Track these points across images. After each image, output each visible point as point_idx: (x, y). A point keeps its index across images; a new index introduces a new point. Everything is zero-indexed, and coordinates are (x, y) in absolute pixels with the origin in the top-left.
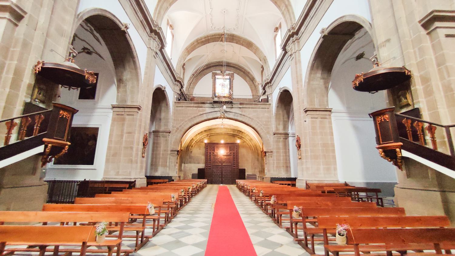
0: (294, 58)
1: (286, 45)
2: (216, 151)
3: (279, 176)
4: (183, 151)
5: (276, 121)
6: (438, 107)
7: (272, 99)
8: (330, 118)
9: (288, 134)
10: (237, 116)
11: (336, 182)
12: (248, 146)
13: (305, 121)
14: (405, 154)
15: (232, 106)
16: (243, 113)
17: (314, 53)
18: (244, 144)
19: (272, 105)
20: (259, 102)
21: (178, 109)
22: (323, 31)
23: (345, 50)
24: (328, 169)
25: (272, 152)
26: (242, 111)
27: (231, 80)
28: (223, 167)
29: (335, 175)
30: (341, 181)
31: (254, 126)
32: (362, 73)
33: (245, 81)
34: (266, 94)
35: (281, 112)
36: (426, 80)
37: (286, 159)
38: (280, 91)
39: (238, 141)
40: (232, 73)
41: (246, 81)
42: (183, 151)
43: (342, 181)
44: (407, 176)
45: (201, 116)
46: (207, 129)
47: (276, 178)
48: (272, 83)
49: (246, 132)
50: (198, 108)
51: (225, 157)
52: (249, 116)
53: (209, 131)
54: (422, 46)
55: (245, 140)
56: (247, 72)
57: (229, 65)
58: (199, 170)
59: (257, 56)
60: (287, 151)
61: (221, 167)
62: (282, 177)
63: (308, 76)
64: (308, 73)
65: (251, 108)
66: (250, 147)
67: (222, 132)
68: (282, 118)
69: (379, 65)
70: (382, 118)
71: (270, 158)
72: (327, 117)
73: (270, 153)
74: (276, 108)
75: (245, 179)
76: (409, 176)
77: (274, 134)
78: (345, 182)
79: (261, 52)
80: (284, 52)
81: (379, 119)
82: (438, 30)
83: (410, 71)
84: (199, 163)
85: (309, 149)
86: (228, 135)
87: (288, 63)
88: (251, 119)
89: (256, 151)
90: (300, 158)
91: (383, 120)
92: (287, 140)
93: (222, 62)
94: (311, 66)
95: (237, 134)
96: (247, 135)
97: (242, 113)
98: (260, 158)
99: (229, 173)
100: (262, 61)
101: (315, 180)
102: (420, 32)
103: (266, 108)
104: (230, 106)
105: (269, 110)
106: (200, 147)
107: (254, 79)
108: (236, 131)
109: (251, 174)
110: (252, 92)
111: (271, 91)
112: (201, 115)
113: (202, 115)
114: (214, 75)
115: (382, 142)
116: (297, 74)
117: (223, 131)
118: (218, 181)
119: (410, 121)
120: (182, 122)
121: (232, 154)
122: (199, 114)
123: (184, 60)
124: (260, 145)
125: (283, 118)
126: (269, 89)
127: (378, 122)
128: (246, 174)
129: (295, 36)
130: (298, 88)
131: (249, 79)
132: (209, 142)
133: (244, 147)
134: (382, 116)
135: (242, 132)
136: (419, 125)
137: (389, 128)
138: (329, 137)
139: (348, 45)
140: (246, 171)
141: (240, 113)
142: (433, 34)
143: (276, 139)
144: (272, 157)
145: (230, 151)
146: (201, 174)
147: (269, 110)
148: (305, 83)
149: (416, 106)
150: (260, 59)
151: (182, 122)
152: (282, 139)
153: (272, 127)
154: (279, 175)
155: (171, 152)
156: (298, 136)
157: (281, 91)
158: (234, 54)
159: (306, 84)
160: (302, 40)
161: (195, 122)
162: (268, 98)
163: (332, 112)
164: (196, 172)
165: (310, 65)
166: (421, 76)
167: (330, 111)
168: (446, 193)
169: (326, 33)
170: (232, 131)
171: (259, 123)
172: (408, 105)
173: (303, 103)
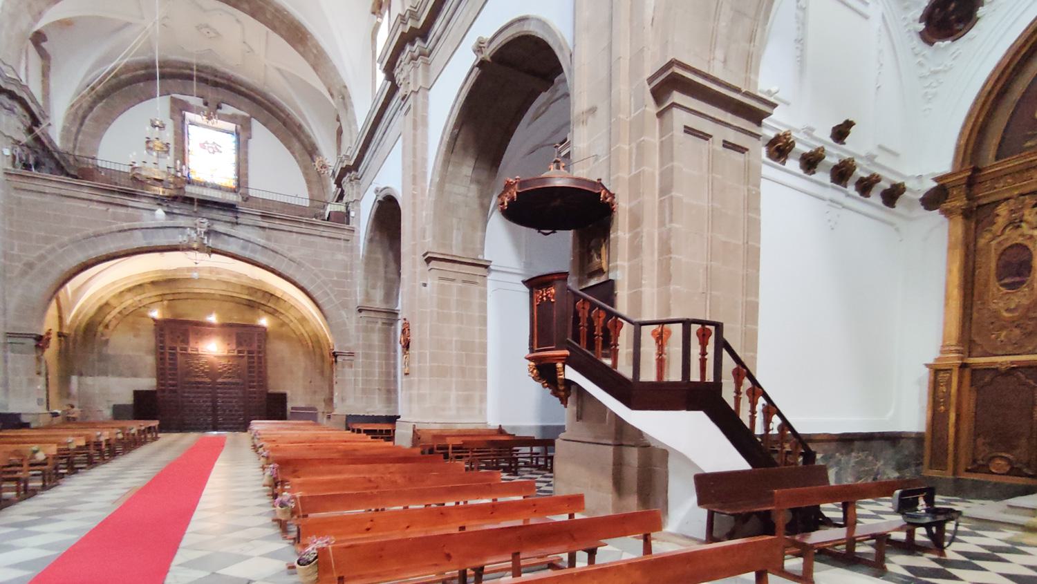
0: (412, 110)
1: (395, 65)
2: (192, 344)
3: (368, 413)
4: (71, 339)
5: (366, 278)
6: (643, 282)
7: (357, 217)
8: (485, 285)
9: (397, 314)
10: (254, 251)
11: (481, 427)
12: (295, 336)
13: (425, 285)
14: (571, 374)
15: (237, 218)
16: (272, 245)
17: (457, 105)
18: (284, 329)
19: (359, 232)
20: (324, 220)
21: (23, 197)
22: (481, 47)
23: (536, 117)
24: (467, 400)
25: (351, 354)
26: (268, 239)
27: (242, 139)
28: (218, 388)
29: (482, 411)
30: (492, 425)
31: (304, 283)
32: (518, 177)
33: (288, 152)
34: (345, 199)
35: (380, 256)
36: (636, 221)
37: (388, 374)
38: (376, 199)
39: (264, 321)
40: (244, 117)
41: (293, 153)
42: (71, 339)
43: (493, 422)
44: (577, 417)
45: (122, 234)
46: (161, 279)
47: (359, 416)
48: (362, 171)
49: (289, 297)
50: (112, 209)
51: (224, 362)
52: (290, 255)
53: (166, 285)
54: (643, 140)
55: (287, 321)
56: (295, 123)
57: (233, 85)
58: (138, 394)
59: (320, 77)
60: (392, 353)
61: (210, 388)
62: (376, 415)
63: (439, 168)
64: (441, 158)
65: (297, 233)
66: (300, 340)
67: (213, 292)
68: (381, 270)
69: (561, 168)
70: (545, 294)
71: (347, 369)
72: (478, 280)
73: (346, 358)
74: (366, 242)
75: (285, 418)
76: (579, 417)
77: (360, 311)
78: (500, 426)
79: (334, 68)
80: (389, 83)
81: (542, 294)
82: (675, 111)
83: (613, 196)
84: (135, 375)
85: (428, 352)
86: (233, 302)
87: (398, 123)
88: (295, 265)
89: (317, 350)
90: (406, 372)
91: (545, 299)
92: (393, 327)
93: (188, 66)
94: (449, 143)
95: (262, 302)
96: (292, 306)
97: (270, 243)
98: (327, 366)
99: (236, 402)
100: (336, 99)
101: (435, 423)
102: (646, 106)
103: (340, 239)
104: (229, 216)
105: (349, 245)
106: (138, 329)
107: (317, 149)
108: (260, 294)
109: (303, 406)
110: (310, 189)
111: (358, 194)
112: (125, 230)
113: (128, 233)
114: (179, 109)
115: (538, 347)
116: (415, 155)
117: (217, 290)
118: (201, 424)
119: (587, 307)
120: (48, 247)
121: (245, 354)
122: (114, 227)
123: (36, 20)
124: (328, 336)
125: (386, 272)
126: (352, 185)
127: (537, 302)
128: (289, 406)
129: (418, 43)
130: (414, 196)
131: (302, 147)
132: (168, 316)
133: (281, 337)
134: (544, 290)
135: (278, 298)
136: (599, 317)
137: (553, 317)
138: (477, 328)
139: (539, 108)
140: (289, 400)
141: (263, 242)
142: (667, 115)
143: (365, 324)
144: (351, 366)
145: (237, 347)
146: (144, 405)
147: (349, 245)
148: (431, 186)
149: (611, 277)
150: (329, 91)
151: (48, 247)
152: (379, 325)
153: (356, 292)
154: (368, 410)
155: (9, 340)
156: (405, 319)
157: (380, 198)
158: (248, 52)
159: (433, 189)
160: (437, 58)
161: (103, 250)
162: (348, 212)
163: (492, 270)
164: (128, 399)
165: (446, 139)
166: (631, 210)
167: (486, 267)
168: (624, 448)
169: (487, 54)
170: (247, 292)
171: (319, 278)
172: (600, 271)
173: (424, 237)
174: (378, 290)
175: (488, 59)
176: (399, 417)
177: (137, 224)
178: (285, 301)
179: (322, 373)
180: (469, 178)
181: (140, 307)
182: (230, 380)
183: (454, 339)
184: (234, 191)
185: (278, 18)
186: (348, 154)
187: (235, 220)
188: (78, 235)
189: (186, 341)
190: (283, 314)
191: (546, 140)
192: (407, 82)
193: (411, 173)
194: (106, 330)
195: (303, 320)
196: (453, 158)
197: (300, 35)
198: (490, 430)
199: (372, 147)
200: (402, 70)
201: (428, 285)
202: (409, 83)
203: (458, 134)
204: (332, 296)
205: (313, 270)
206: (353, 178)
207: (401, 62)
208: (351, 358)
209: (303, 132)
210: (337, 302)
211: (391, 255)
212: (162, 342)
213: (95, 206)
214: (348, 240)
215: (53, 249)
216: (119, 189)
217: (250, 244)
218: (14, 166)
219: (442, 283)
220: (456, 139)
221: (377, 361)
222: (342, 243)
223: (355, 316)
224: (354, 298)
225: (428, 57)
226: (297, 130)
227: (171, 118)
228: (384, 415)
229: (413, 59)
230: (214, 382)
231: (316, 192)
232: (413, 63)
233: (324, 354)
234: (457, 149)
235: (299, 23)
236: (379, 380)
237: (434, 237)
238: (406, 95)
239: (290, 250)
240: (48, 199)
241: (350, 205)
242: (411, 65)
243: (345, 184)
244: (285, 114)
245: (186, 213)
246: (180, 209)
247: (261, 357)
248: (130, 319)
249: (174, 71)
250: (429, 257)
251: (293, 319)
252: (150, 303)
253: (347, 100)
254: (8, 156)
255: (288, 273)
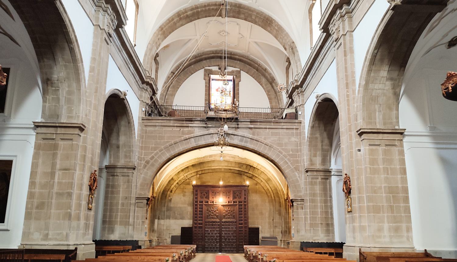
3: (314, 241)
5: (310, 151)
8: (402, 146)
11: (410, 251)
13: (359, 150)
15: (238, 124)
16: (255, 137)
18: (257, 186)
19: (304, 123)
24: (397, 229)
25: (302, 200)
26: (254, 134)
28: (223, 225)
29: (409, 239)
31: (273, 157)
34: (295, 105)
35: (318, 135)
40: (237, 71)
52: (265, 142)
53: (199, 165)
55: (259, 181)
57: (233, 56)
61: (218, 225)
63: (364, 76)
64: (366, 69)
65: (269, 128)
66: (267, 193)
67: (221, 167)
73: (299, 203)
77: (307, 172)
78: (426, 250)
84: (182, 218)
88: (268, 147)
89: (277, 199)
90: (349, 210)
92: (328, 181)
101: (375, 247)
104: (234, 125)
105: (298, 132)
107: (275, 80)
108: (244, 166)
110: (271, 103)
111: (303, 100)
114: (208, 73)
117: (223, 166)
125: (322, 145)
126: (299, 96)
132: (199, 184)
135: (254, 168)
138: (399, 176)
140: (260, 232)
141: (251, 136)
147: (298, 132)
148: (359, 87)
150: (284, 47)
152: (319, 180)
153: (304, 159)
154: (315, 238)
156: (346, 174)
157: (319, 101)
160: (357, 14)
161: (177, 151)
162: (297, 112)
164: (178, 233)
165: (369, 57)
167: (402, 134)
171: (282, 153)
174: (318, 157)
175: (400, 3)
176: (344, 243)
177: (192, 135)
178: (258, 169)
179: (280, 214)
180: (385, 78)
181: (187, 180)
182: (229, 220)
183: (383, 185)
184: (232, 111)
185: (258, 17)
186: (296, 79)
187: (237, 126)
188: (167, 144)
189: (208, 197)
190: (257, 177)
191: (440, 41)
192: (338, 30)
193: (345, 82)
194: (171, 193)
195: (268, 180)
196: (374, 68)
197: (269, 22)
198: (418, 253)
199: (312, 72)
200: (334, 24)
201: (361, 151)
202: (339, 31)
203: (377, 53)
204: (289, 164)
205: (278, 149)
206: (299, 92)
207: (334, 20)
208: (302, 203)
209: (267, 72)
210: (292, 167)
211: (325, 135)
212: (196, 198)
213: (175, 129)
214: (298, 129)
215: (157, 153)
216: (185, 118)
217: (245, 138)
218: (146, 116)
219: (371, 148)
220: (375, 56)
221: (319, 204)
222: (294, 131)
223: (303, 175)
224: (302, 164)
225: (351, 13)
226: (264, 72)
227: (204, 79)
228: (325, 242)
229: (341, 17)
230: (221, 222)
231: (274, 104)
232: (342, 19)
233: (281, 201)
234: (377, 61)
235: (269, 16)
236: (321, 217)
237: (364, 119)
238: (338, 38)
239: (265, 139)
240: (157, 128)
241: (298, 108)
242: (341, 20)
243: (294, 96)
244: (257, 64)
245: (214, 126)
246: (211, 124)
247: (246, 205)
248: (182, 186)
249: (207, 56)
250: (361, 132)
251: (262, 180)
252: (191, 177)
253: (294, 50)
254: (143, 111)
255: (264, 152)
